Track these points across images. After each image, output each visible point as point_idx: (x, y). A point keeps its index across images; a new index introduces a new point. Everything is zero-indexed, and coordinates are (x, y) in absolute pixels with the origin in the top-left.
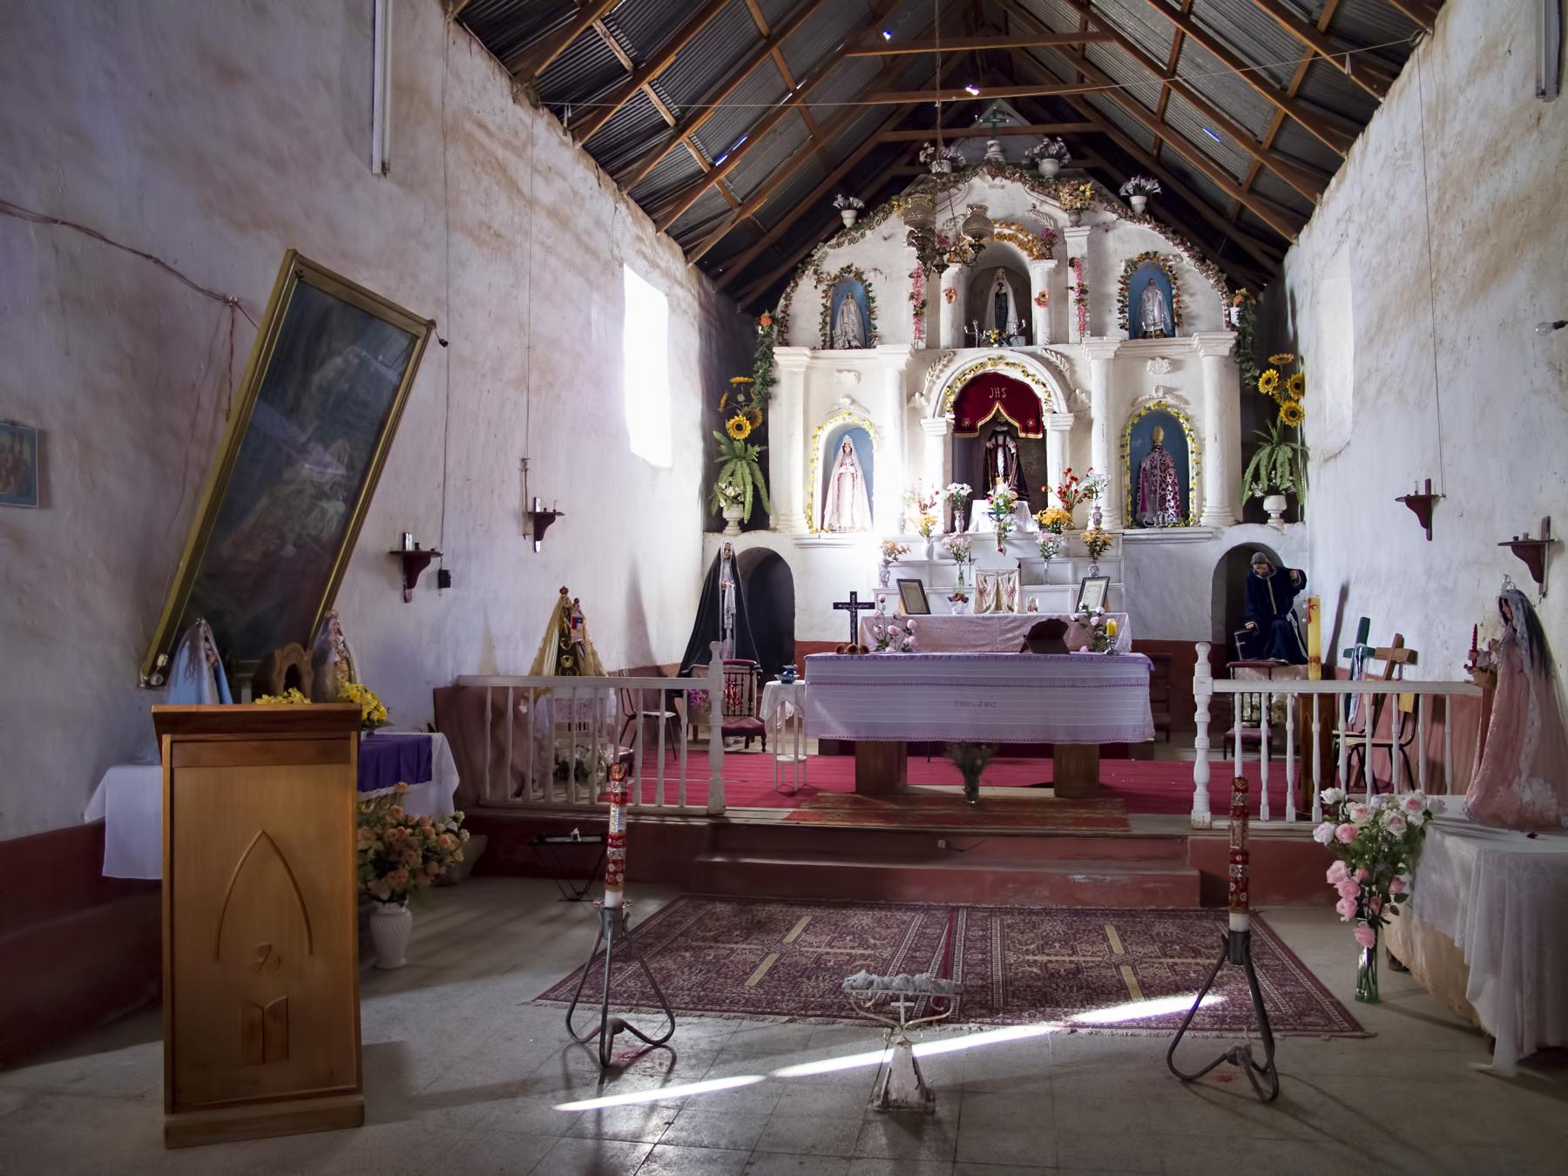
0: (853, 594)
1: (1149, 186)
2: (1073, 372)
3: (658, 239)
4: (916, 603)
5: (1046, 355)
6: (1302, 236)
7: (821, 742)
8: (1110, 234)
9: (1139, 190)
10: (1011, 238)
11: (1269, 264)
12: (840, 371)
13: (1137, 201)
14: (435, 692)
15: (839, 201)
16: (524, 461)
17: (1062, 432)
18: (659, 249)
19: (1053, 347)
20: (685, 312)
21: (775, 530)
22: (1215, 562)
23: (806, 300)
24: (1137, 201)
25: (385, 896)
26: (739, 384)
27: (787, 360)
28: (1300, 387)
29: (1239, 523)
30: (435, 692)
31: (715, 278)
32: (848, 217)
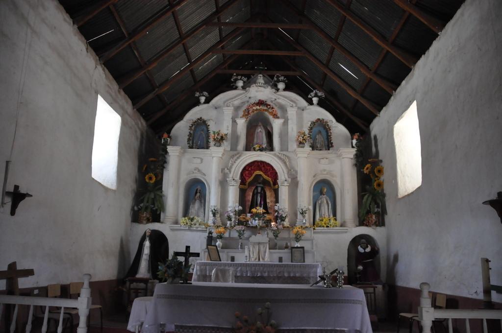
0: (188, 248)
1: (320, 94)
2: (290, 162)
3: (119, 92)
4: (214, 255)
5: (280, 155)
6: (382, 112)
7: (175, 326)
8: (305, 111)
9: (316, 95)
10: (266, 110)
11: (364, 127)
12: (194, 158)
13: (315, 100)
14: (34, 275)
15: (197, 94)
16: (7, 162)
17: (352, 159)
18: (119, 96)
19: (282, 152)
20: (131, 128)
21: (162, 223)
22: (348, 243)
23: (182, 128)
24: (315, 100)
25: (257, 148)
26: (152, 161)
27: (173, 152)
28: (380, 171)
29: (357, 226)
30: (34, 275)
31: (146, 118)
32: (203, 99)
